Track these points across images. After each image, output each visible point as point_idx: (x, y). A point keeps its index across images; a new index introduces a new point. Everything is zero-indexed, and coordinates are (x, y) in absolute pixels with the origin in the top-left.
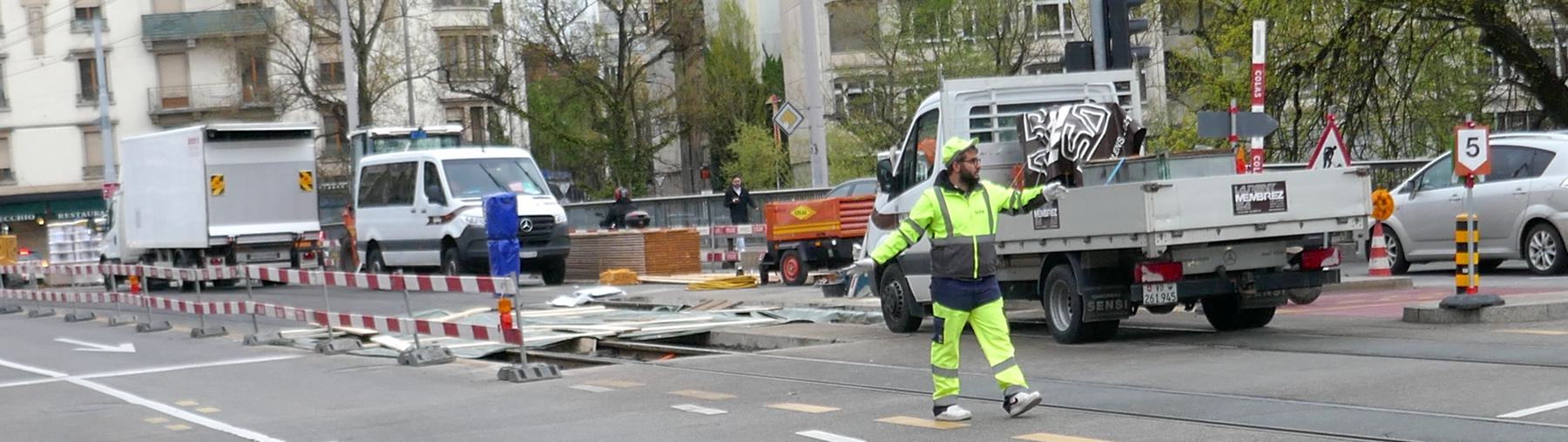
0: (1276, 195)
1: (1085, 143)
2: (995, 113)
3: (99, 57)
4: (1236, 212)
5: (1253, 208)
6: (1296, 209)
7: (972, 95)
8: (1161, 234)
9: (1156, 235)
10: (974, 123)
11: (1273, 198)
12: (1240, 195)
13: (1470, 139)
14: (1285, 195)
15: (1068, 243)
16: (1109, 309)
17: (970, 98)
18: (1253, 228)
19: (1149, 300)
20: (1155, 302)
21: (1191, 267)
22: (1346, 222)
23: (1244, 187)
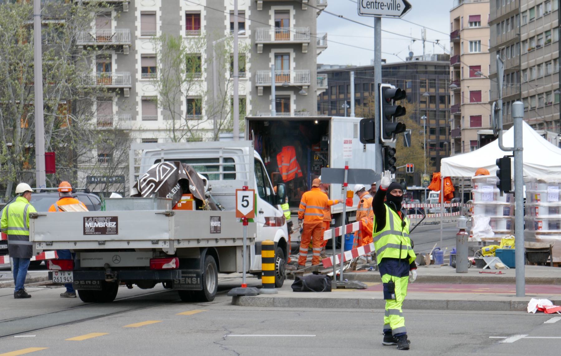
0: (112, 225)
1: (152, 186)
2: (221, 163)
3: (188, 98)
4: (85, 233)
5: (95, 232)
6: (123, 234)
7: (156, 153)
8: (40, 243)
9: (37, 244)
10: (234, 168)
11: (109, 226)
12: (88, 223)
13: (244, 197)
14: (117, 225)
15: (41, 245)
16: (188, 283)
17: (154, 155)
18: (97, 243)
19: (56, 280)
20: (60, 281)
21: (85, 264)
22: (52, 245)
23: (91, 219)
